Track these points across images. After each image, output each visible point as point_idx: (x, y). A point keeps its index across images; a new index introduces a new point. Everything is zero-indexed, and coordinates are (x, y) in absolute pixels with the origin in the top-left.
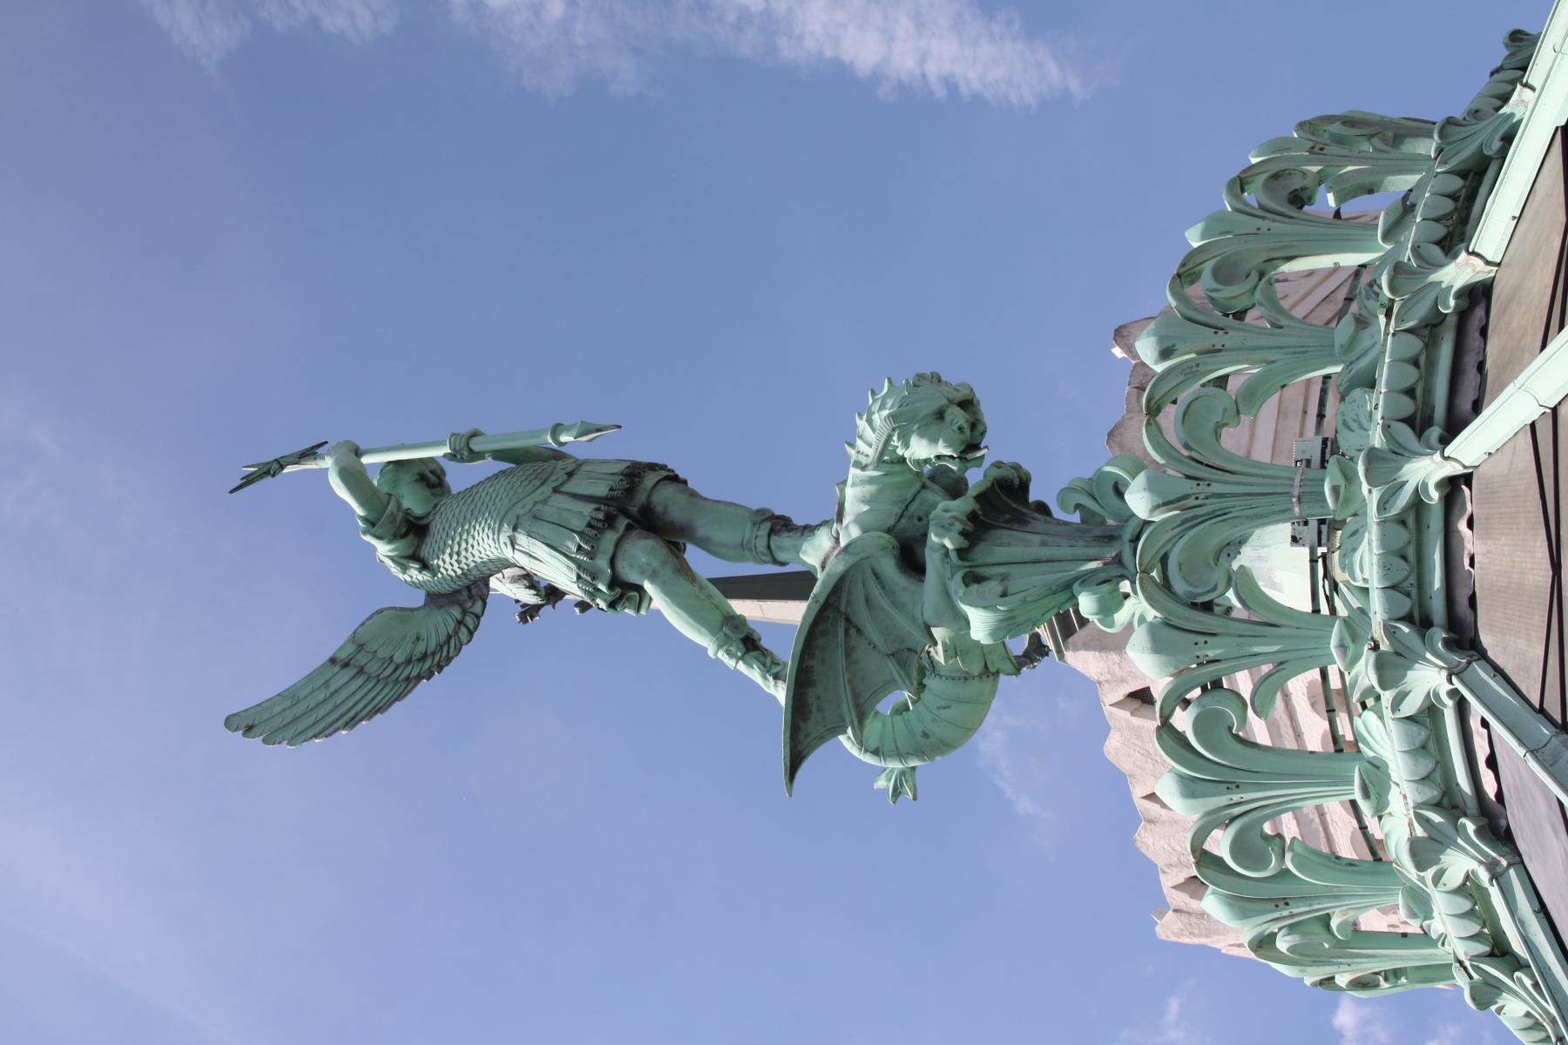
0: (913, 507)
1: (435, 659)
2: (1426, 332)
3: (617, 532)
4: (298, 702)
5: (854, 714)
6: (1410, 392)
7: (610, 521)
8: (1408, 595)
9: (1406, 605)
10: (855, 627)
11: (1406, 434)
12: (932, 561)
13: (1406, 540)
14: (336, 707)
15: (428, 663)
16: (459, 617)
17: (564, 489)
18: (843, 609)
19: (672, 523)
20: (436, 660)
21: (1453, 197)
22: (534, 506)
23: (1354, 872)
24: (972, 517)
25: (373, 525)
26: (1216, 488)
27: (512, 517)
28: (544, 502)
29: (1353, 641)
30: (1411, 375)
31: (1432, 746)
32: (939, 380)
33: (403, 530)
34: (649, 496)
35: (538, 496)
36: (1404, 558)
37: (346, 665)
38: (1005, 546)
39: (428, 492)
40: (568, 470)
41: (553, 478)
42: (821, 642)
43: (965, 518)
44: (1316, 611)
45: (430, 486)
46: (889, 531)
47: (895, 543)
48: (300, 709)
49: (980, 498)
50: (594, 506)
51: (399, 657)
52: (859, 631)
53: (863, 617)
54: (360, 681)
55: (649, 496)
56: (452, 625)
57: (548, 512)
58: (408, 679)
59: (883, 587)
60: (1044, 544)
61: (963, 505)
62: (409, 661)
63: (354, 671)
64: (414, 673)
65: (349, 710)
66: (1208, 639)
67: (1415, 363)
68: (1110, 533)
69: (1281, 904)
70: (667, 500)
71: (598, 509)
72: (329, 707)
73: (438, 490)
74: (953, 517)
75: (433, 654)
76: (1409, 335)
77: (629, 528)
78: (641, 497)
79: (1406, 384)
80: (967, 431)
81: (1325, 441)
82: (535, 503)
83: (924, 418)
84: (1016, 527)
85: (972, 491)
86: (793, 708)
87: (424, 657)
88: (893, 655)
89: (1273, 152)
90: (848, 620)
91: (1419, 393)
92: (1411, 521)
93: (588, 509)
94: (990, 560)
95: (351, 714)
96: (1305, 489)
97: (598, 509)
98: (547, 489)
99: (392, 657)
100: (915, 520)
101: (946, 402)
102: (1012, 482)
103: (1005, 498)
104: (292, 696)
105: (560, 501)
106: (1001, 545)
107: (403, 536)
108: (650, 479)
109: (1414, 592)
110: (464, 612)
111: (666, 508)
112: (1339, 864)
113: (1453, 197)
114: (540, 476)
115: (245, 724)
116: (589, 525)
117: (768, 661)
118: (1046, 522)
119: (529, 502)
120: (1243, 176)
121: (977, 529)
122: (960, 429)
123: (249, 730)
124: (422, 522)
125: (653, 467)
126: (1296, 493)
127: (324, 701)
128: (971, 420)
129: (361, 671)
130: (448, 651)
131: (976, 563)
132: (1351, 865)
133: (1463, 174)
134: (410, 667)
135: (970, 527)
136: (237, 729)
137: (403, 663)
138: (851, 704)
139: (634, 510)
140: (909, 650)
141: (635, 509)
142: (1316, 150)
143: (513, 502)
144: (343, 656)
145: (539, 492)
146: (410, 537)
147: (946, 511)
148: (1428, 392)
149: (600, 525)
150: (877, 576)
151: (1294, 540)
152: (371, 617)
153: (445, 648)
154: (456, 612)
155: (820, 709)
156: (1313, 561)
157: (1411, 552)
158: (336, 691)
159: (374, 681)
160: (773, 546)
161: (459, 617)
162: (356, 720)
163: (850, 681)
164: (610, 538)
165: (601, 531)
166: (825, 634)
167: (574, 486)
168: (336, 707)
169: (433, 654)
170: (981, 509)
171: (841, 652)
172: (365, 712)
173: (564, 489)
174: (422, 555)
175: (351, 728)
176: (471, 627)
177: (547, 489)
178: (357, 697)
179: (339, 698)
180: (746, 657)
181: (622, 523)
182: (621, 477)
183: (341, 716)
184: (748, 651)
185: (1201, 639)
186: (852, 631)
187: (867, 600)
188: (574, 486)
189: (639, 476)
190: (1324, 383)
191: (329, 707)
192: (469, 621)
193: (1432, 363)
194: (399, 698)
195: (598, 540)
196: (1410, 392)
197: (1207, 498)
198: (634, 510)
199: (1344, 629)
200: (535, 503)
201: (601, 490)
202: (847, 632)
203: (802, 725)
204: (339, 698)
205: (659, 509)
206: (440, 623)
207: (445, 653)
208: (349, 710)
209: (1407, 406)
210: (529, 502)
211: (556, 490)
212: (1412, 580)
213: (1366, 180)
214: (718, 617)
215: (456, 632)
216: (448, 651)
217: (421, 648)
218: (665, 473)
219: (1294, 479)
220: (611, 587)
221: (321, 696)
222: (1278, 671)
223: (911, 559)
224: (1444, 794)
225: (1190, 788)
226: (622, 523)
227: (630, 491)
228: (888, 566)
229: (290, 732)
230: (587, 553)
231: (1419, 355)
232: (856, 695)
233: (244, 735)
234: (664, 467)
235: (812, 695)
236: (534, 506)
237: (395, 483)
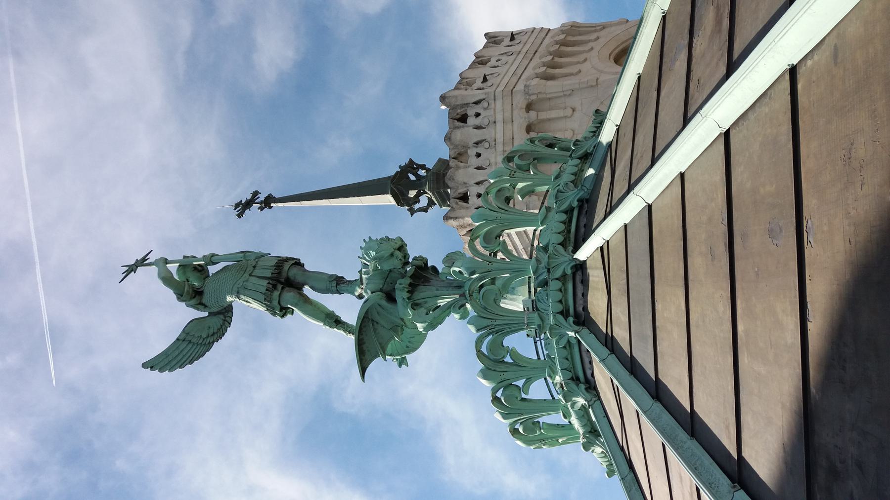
0: (388, 280)
1: (219, 333)
2: (562, 279)
3: (278, 291)
4: (168, 355)
5: (381, 351)
6: (560, 301)
7: (275, 287)
8: (571, 371)
9: (570, 375)
10: (375, 322)
11: (561, 318)
12: (399, 300)
13: (567, 354)
14: (184, 356)
15: (216, 336)
16: (224, 319)
17: (253, 274)
18: (370, 318)
19: (299, 283)
20: (219, 335)
21: (564, 223)
22: (243, 283)
23: (564, 430)
24: (410, 285)
25: (182, 296)
26: (498, 322)
27: (235, 289)
28: (247, 281)
29: (554, 374)
30: (559, 296)
31: (586, 416)
32: (389, 239)
33: (194, 295)
34: (287, 274)
35: (243, 279)
36: (567, 359)
37: (184, 340)
38: (422, 293)
39: (199, 274)
40: (253, 265)
41: (248, 270)
42: (364, 329)
43: (408, 286)
44: (539, 359)
45: (200, 271)
46: (381, 290)
47: (385, 295)
48: (170, 358)
49: (411, 277)
50: (268, 281)
51: (204, 336)
52: (377, 323)
53: (377, 318)
54: (190, 346)
55: (287, 274)
56: (221, 322)
57: (249, 285)
58: (209, 343)
59: (383, 309)
60: (437, 290)
61: (408, 281)
62: (208, 336)
63: (188, 342)
64: (211, 341)
65: (189, 357)
66: (504, 373)
67: (560, 290)
68: (460, 285)
69: (542, 441)
70: (294, 273)
71: (269, 283)
72: (181, 356)
73: (203, 272)
74: (403, 287)
75: (217, 333)
76: (557, 281)
77: (283, 288)
78: (284, 275)
79: (564, 356)
80: (403, 260)
81: (533, 301)
82: (244, 282)
83: (386, 257)
84: (426, 284)
85: (409, 274)
86: (359, 354)
87: (214, 334)
88: (391, 329)
89: (497, 178)
90: (372, 320)
91: (563, 301)
92: (568, 347)
93: (265, 283)
94: (419, 298)
95: (191, 358)
96: (528, 321)
97: (269, 283)
98: (247, 275)
99: (201, 336)
100: (390, 284)
101: (393, 250)
102: (422, 266)
103: (420, 271)
104: (165, 354)
105: (253, 280)
106: (422, 292)
107: (194, 297)
108: (286, 266)
109: (570, 359)
110: (225, 317)
111: (295, 277)
112: (559, 427)
113: (564, 223)
114: (242, 269)
115: (150, 366)
116: (267, 290)
117: (346, 326)
118: (437, 280)
119: (241, 282)
120: (487, 191)
121: (412, 288)
122: (400, 259)
123: (152, 368)
124: (199, 290)
125: (287, 259)
126: (526, 322)
127: (179, 354)
128: (403, 255)
129: (190, 342)
130: (222, 332)
131: (415, 299)
132: (563, 427)
133: (566, 212)
134: (209, 338)
135: (410, 289)
136: (147, 368)
137: (206, 338)
138: (379, 347)
139: (283, 280)
140: (396, 326)
141: (283, 280)
142: (511, 175)
143: (235, 282)
144: (182, 338)
145: (243, 276)
146: (197, 297)
147: (400, 284)
148: (566, 301)
149: (271, 290)
150: (380, 306)
151: (528, 335)
152: (188, 324)
153: (221, 330)
154: (222, 317)
155: (368, 351)
156: (535, 343)
157: (569, 357)
158: (183, 350)
159: (196, 345)
160: (339, 290)
161: (224, 319)
162: (193, 360)
163: (377, 340)
164: (276, 294)
165: (272, 292)
166: (365, 326)
167: (257, 272)
168: (184, 356)
169: (217, 333)
170: (413, 281)
171: (372, 331)
172: (196, 356)
173: (253, 274)
174: (203, 302)
175: (192, 364)
176: (229, 322)
177: (247, 275)
178: (191, 352)
179: (184, 353)
180: (337, 327)
181: (280, 287)
182: (275, 267)
183: (187, 359)
184: (337, 325)
185: (502, 374)
186: (375, 324)
187: (378, 313)
188: (257, 272)
189: (282, 266)
190: (529, 279)
191: (181, 356)
192: (228, 319)
193: (566, 290)
194: (208, 351)
195: (272, 295)
196: (560, 301)
197: (495, 326)
198: (283, 280)
199: (549, 370)
200: (244, 282)
201: (268, 274)
202: (373, 325)
203: (363, 358)
204: (184, 353)
205: (292, 278)
206: (217, 321)
207: (221, 332)
208: (189, 357)
209: (560, 307)
210: (241, 282)
211: (250, 275)
212: (571, 366)
213: (531, 189)
214: (323, 316)
215: (224, 324)
216: (222, 332)
217: (211, 331)
218: (293, 262)
219: (524, 318)
220: (281, 311)
221: (177, 353)
222: (527, 382)
223: (390, 298)
224: (592, 429)
225: (505, 416)
226: (280, 287)
227: (279, 273)
228: (384, 303)
229: (169, 367)
230: (269, 301)
231: (561, 287)
232: (380, 344)
233: (151, 370)
234: (293, 259)
235: (365, 347)
236: (243, 283)
237: (184, 273)
